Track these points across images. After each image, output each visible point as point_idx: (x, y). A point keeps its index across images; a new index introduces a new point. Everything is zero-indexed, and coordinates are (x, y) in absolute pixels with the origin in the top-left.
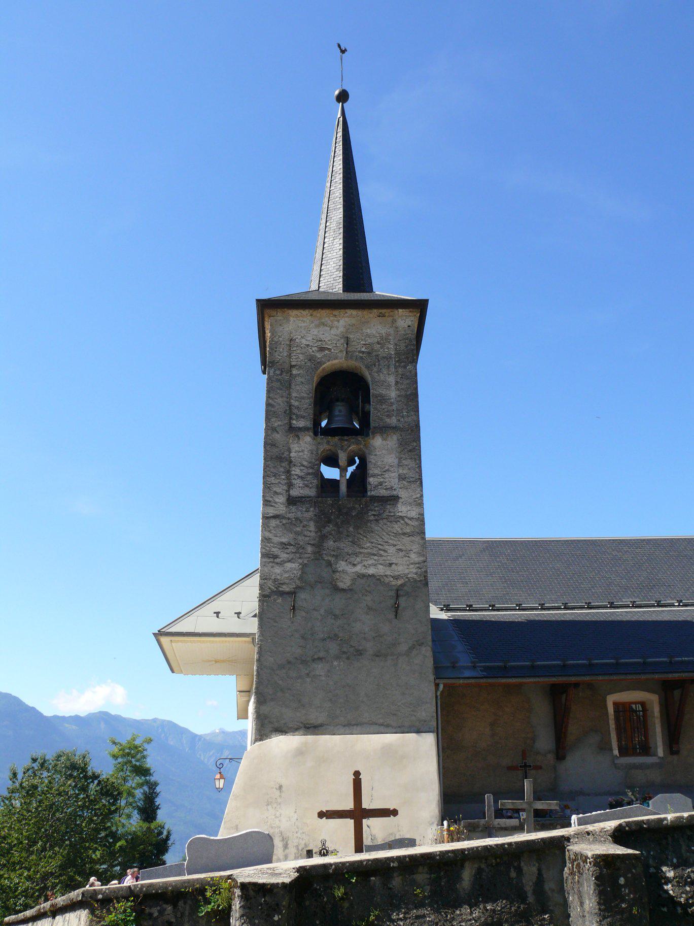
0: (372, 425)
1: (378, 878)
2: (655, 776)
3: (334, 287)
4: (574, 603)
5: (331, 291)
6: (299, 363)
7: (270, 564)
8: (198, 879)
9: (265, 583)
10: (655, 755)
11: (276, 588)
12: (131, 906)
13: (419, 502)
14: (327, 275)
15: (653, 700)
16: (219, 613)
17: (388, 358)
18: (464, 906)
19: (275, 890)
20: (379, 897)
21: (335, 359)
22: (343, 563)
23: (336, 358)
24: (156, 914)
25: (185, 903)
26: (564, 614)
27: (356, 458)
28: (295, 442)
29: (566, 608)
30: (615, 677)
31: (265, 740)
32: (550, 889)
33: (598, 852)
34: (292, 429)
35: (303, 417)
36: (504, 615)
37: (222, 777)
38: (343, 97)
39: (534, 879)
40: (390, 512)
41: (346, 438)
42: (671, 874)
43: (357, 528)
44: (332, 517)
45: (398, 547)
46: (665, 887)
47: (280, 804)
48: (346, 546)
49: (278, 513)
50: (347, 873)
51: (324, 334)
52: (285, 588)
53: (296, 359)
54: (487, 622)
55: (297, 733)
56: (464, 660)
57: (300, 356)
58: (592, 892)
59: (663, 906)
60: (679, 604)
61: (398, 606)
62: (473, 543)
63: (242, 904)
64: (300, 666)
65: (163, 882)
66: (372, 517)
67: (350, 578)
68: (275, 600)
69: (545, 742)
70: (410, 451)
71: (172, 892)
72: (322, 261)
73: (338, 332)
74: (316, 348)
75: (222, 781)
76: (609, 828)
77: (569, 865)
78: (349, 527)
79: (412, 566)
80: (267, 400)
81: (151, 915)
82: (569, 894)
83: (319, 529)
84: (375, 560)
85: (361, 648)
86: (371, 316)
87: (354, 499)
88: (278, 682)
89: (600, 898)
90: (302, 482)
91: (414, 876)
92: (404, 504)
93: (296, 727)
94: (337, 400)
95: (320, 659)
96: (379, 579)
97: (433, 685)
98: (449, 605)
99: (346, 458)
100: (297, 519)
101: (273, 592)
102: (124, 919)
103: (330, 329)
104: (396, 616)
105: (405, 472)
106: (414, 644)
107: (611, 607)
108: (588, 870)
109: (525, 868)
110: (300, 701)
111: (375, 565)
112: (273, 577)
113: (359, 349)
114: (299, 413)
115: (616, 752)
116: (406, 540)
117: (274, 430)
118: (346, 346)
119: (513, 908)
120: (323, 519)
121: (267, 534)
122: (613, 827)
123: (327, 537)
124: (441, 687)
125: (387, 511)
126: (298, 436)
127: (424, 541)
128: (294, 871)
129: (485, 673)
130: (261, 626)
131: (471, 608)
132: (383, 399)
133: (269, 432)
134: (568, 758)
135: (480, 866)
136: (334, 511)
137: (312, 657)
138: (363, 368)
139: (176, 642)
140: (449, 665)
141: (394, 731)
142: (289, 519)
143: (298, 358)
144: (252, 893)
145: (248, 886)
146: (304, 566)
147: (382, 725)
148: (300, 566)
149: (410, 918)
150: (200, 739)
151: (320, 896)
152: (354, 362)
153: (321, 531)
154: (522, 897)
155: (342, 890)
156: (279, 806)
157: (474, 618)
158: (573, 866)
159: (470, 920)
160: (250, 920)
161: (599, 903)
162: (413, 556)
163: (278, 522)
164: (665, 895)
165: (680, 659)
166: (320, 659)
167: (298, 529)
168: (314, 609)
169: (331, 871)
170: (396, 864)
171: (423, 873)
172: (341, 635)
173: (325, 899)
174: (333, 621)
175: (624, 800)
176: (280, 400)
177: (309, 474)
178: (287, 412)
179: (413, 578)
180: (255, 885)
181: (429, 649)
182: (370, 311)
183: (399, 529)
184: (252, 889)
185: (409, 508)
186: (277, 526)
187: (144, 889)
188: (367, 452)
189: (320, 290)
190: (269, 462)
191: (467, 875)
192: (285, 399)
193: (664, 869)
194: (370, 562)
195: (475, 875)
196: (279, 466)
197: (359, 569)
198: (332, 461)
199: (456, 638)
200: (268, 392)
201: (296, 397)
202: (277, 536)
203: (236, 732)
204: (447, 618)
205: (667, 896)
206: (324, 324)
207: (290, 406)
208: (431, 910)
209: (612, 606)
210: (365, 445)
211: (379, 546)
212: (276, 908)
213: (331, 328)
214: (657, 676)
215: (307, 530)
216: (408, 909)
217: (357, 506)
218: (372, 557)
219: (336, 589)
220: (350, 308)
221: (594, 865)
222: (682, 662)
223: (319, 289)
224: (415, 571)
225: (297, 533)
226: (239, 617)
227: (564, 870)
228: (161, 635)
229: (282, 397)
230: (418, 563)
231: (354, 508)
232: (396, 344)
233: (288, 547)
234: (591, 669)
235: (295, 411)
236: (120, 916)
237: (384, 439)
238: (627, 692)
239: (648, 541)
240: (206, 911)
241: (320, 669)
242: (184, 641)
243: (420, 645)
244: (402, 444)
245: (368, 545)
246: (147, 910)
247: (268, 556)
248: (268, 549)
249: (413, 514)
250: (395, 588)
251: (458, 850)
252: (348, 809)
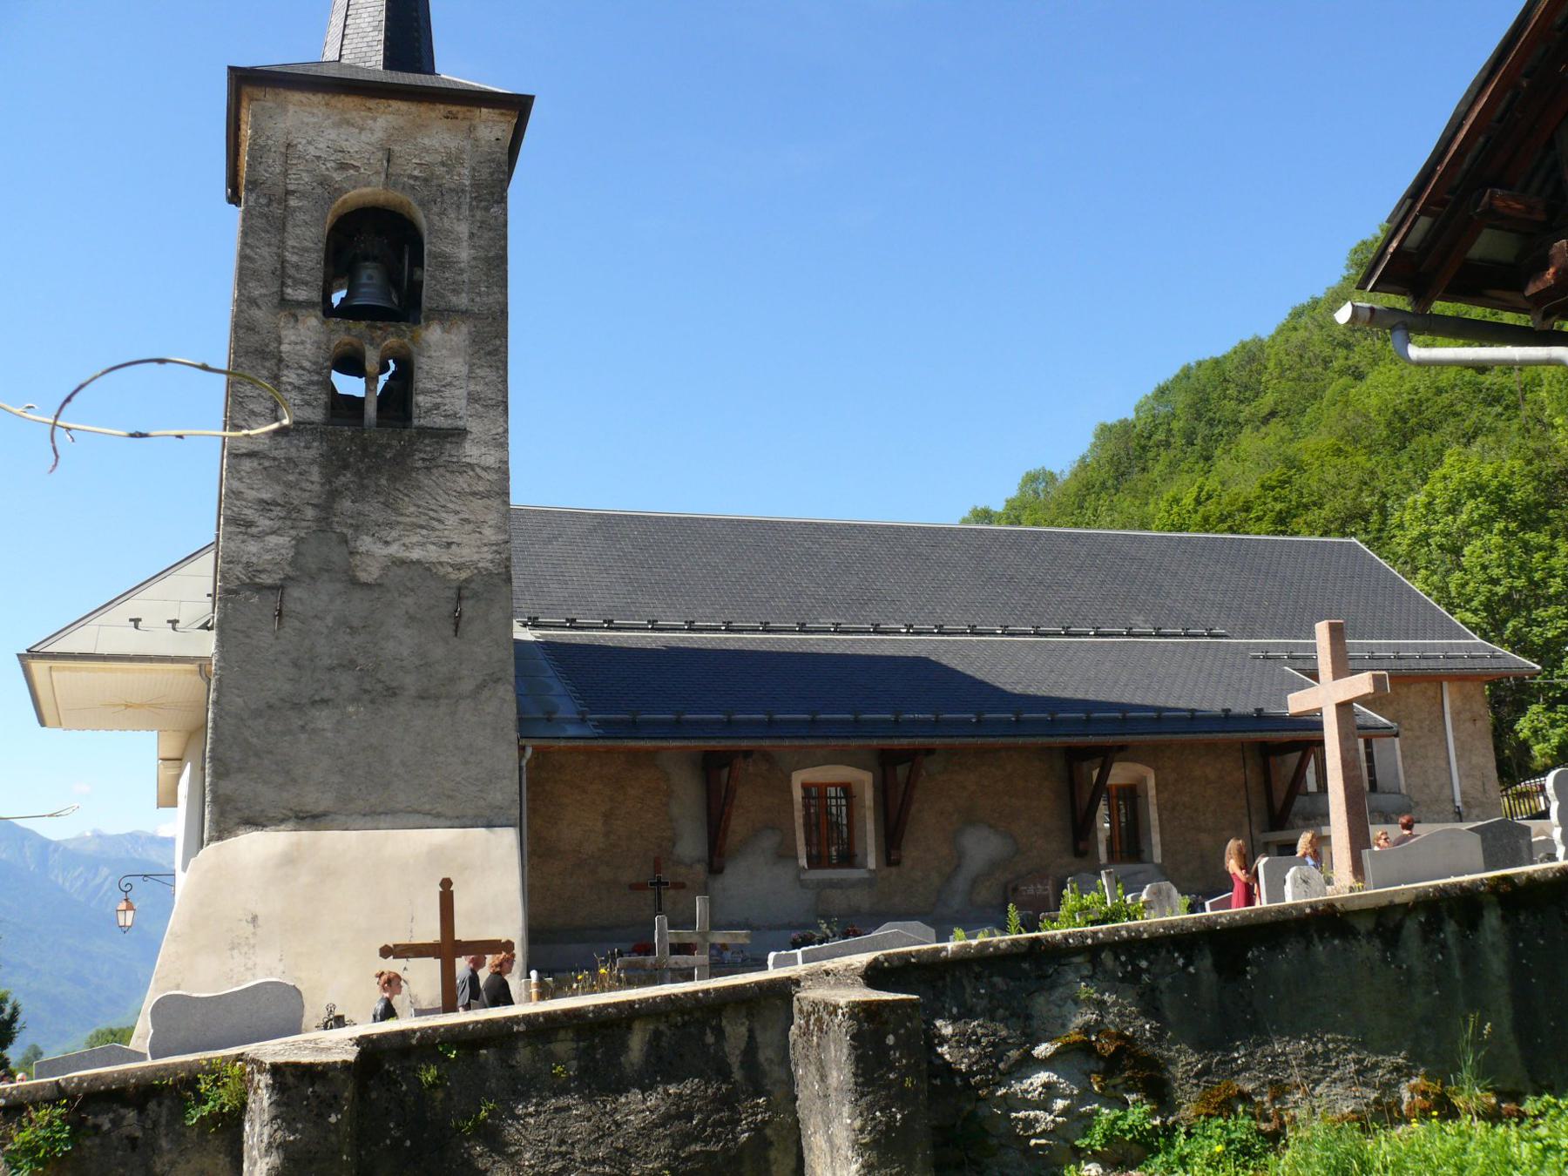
0: (426, 303)
1: (492, 1050)
2: (862, 900)
3: (366, 59)
4: (742, 622)
5: (362, 65)
6: (301, 187)
7: (240, 536)
8: (182, 1064)
9: (229, 569)
10: (863, 866)
11: (249, 578)
12: (62, 1115)
13: (501, 442)
14: (355, 36)
15: (864, 780)
16: (140, 620)
17: (458, 191)
18: (633, 1090)
19: (330, 1074)
20: (494, 1081)
21: (365, 186)
22: (368, 539)
23: (368, 184)
24: (107, 1126)
25: (160, 1104)
26: (727, 639)
27: (391, 362)
28: (290, 326)
29: (728, 630)
30: (811, 743)
31: (226, 838)
32: (766, 1059)
33: (853, 999)
34: (284, 303)
35: (306, 283)
36: (629, 637)
37: (130, 907)
39: (743, 1046)
40: (450, 456)
41: (379, 324)
42: (948, 1030)
43: (393, 479)
44: (351, 460)
46: (939, 1050)
47: (253, 947)
48: (373, 509)
49: (256, 449)
50: (441, 1043)
51: (347, 140)
52: (266, 579)
53: (296, 179)
54: (601, 647)
55: (282, 827)
56: (566, 708)
57: (304, 174)
58: (844, 1058)
59: (936, 1078)
60: (908, 629)
61: (460, 614)
62: (575, 516)
63: (274, 1098)
64: (288, 713)
65: (119, 1072)
66: (420, 462)
67: (378, 565)
68: (247, 599)
69: (691, 845)
70: (489, 353)
71: (136, 1086)
72: (348, 10)
73: (373, 139)
74: (333, 164)
75: (130, 914)
76: (858, 965)
77: (799, 1021)
78: (378, 479)
79: (486, 549)
80: (242, 249)
81: (97, 1127)
82: (796, 1065)
83: (328, 479)
84: (423, 536)
85: (394, 684)
86: (433, 115)
87: (390, 430)
88: (251, 740)
89: (857, 1067)
90: (300, 397)
91: (552, 1046)
92: (476, 442)
93: (281, 816)
94: (366, 259)
95: (324, 701)
96: (429, 569)
97: (515, 747)
98: (537, 618)
99: (378, 359)
100: (289, 460)
101: (244, 584)
102: (49, 1138)
103: (360, 133)
104: (456, 631)
105: (478, 388)
106: (485, 680)
107: (800, 631)
108: (839, 1026)
109: (728, 1029)
110: (288, 772)
111: (423, 544)
112: (244, 560)
113: (409, 172)
114: (298, 276)
115: (803, 862)
116: (478, 504)
117: (253, 302)
118: (385, 164)
119: (709, 1091)
120: (336, 463)
121: (236, 484)
122: (865, 963)
123: (341, 493)
124: (529, 752)
125: (447, 454)
126: (295, 317)
127: (507, 508)
128: (351, 1043)
129: (601, 731)
130: (222, 643)
131: (572, 624)
132: (445, 262)
133: (244, 306)
134: (728, 871)
135: (657, 1028)
136: (354, 448)
137: (310, 699)
138: (414, 205)
139: (58, 669)
140: (541, 716)
141: (449, 823)
142: (274, 459)
143: (301, 178)
144: (290, 1080)
145: (284, 1069)
146: (299, 541)
147: (428, 813)
148: (293, 542)
149: (545, 1112)
150: (55, 850)
151: (396, 1082)
152: (399, 195)
153: (330, 482)
154: (723, 1073)
155: (434, 1071)
156: (251, 951)
157: (579, 641)
158: (807, 1023)
159: (643, 1111)
160: (289, 1124)
161: (855, 1075)
162: (488, 532)
163: (255, 464)
164: (938, 1062)
165: (912, 716)
166: (324, 701)
167: (291, 478)
168: (316, 616)
169: (414, 1042)
170: (522, 1028)
171: (566, 1040)
172: (361, 661)
173: (404, 1088)
174: (348, 638)
175: (814, 936)
176: (265, 251)
177: (311, 383)
178: (278, 273)
179: (486, 569)
180: (296, 1065)
181: (511, 688)
182: (431, 106)
183: (465, 486)
184: (292, 1074)
185: (483, 450)
186: (254, 471)
187: (85, 1084)
188: (415, 349)
189: (342, 61)
190: (242, 359)
191: (637, 1042)
192: (275, 249)
193: (939, 1023)
194: (415, 539)
195: (650, 1042)
196: (259, 367)
197: (394, 549)
198: (351, 363)
199: (550, 673)
200: (245, 234)
201: (293, 247)
202: (253, 489)
203: (123, 836)
204: (533, 639)
205: (941, 1062)
206: (349, 123)
207: (283, 262)
208: (580, 1098)
209: (803, 629)
210: (412, 339)
211: (431, 513)
212: (332, 1103)
213: (362, 129)
214: (875, 742)
215: (307, 480)
216: (542, 1098)
217: (395, 443)
218: (418, 530)
219: (355, 582)
220: (396, 99)
221: (850, 1018)
222: (914, 721)
223: (339, 61)
224: (490, 557)
225: (289, 485)
226: (174, 629)
227: (789, 1030)
228: (33, 657)
229: (269, 245)
230: (496, 545)
231: (389, 446)
232: (474, 169)
233: (272, 508)
234: (771, 728)
235: (291, 271)
236: (42, 1133)
237: (445, 331)
238: (811, 769)
239: (862, 528)
240: (198, 1116)
241: (323, 719)
242: (75, 670)
243: (495, 682)
244: (477, 341)
245: (412, 509)
246: (91, 1120)
247: (235, 521)
248: (235, 509)
249: (490, 460)
250: (455, 584)
251: (623, 1003)
252: (432, 942)
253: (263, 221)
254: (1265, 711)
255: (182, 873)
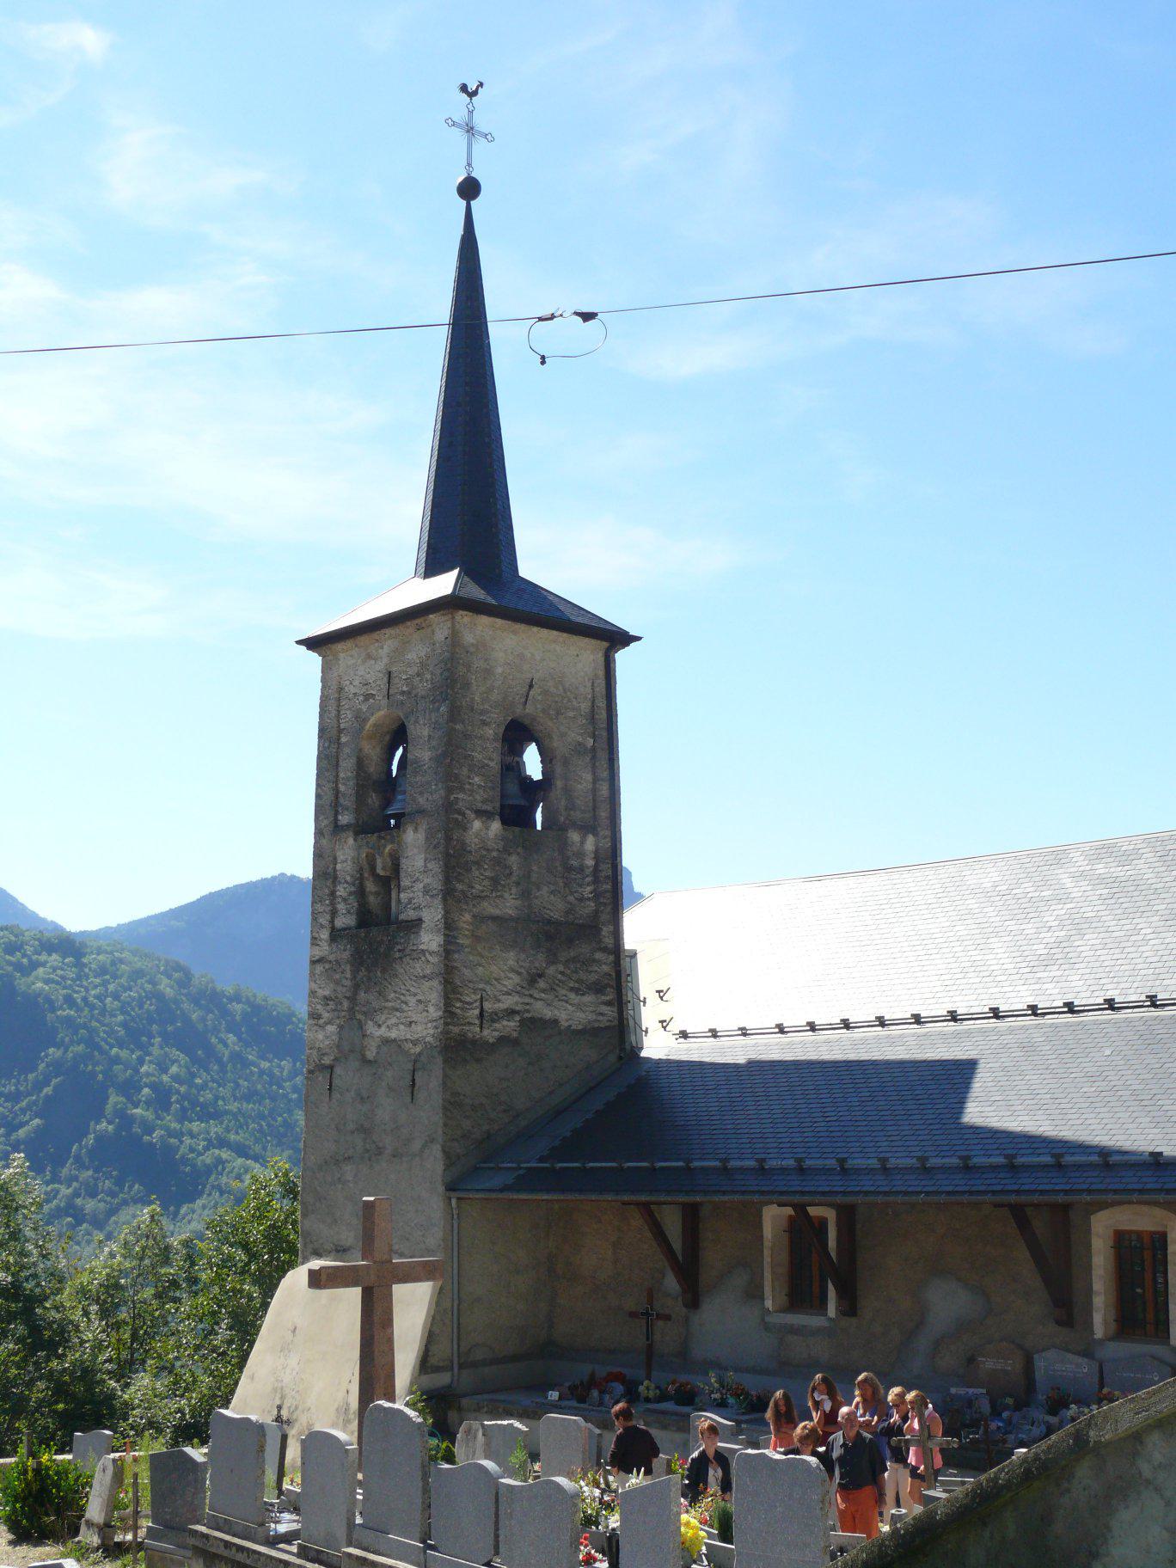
38: (470, 189)
45: (419, 997)
83: (355, 972)
85: (381, 1145)
146: (341, 1027)
167: (338, 976)
219: (365, 1062)
245: (393, 995)
253: (326, 762)
254: (1165, 1154)
255: (305, 1279)
